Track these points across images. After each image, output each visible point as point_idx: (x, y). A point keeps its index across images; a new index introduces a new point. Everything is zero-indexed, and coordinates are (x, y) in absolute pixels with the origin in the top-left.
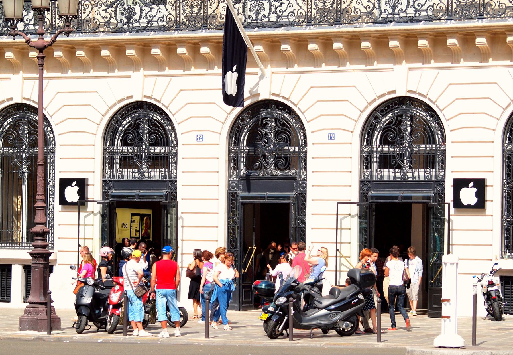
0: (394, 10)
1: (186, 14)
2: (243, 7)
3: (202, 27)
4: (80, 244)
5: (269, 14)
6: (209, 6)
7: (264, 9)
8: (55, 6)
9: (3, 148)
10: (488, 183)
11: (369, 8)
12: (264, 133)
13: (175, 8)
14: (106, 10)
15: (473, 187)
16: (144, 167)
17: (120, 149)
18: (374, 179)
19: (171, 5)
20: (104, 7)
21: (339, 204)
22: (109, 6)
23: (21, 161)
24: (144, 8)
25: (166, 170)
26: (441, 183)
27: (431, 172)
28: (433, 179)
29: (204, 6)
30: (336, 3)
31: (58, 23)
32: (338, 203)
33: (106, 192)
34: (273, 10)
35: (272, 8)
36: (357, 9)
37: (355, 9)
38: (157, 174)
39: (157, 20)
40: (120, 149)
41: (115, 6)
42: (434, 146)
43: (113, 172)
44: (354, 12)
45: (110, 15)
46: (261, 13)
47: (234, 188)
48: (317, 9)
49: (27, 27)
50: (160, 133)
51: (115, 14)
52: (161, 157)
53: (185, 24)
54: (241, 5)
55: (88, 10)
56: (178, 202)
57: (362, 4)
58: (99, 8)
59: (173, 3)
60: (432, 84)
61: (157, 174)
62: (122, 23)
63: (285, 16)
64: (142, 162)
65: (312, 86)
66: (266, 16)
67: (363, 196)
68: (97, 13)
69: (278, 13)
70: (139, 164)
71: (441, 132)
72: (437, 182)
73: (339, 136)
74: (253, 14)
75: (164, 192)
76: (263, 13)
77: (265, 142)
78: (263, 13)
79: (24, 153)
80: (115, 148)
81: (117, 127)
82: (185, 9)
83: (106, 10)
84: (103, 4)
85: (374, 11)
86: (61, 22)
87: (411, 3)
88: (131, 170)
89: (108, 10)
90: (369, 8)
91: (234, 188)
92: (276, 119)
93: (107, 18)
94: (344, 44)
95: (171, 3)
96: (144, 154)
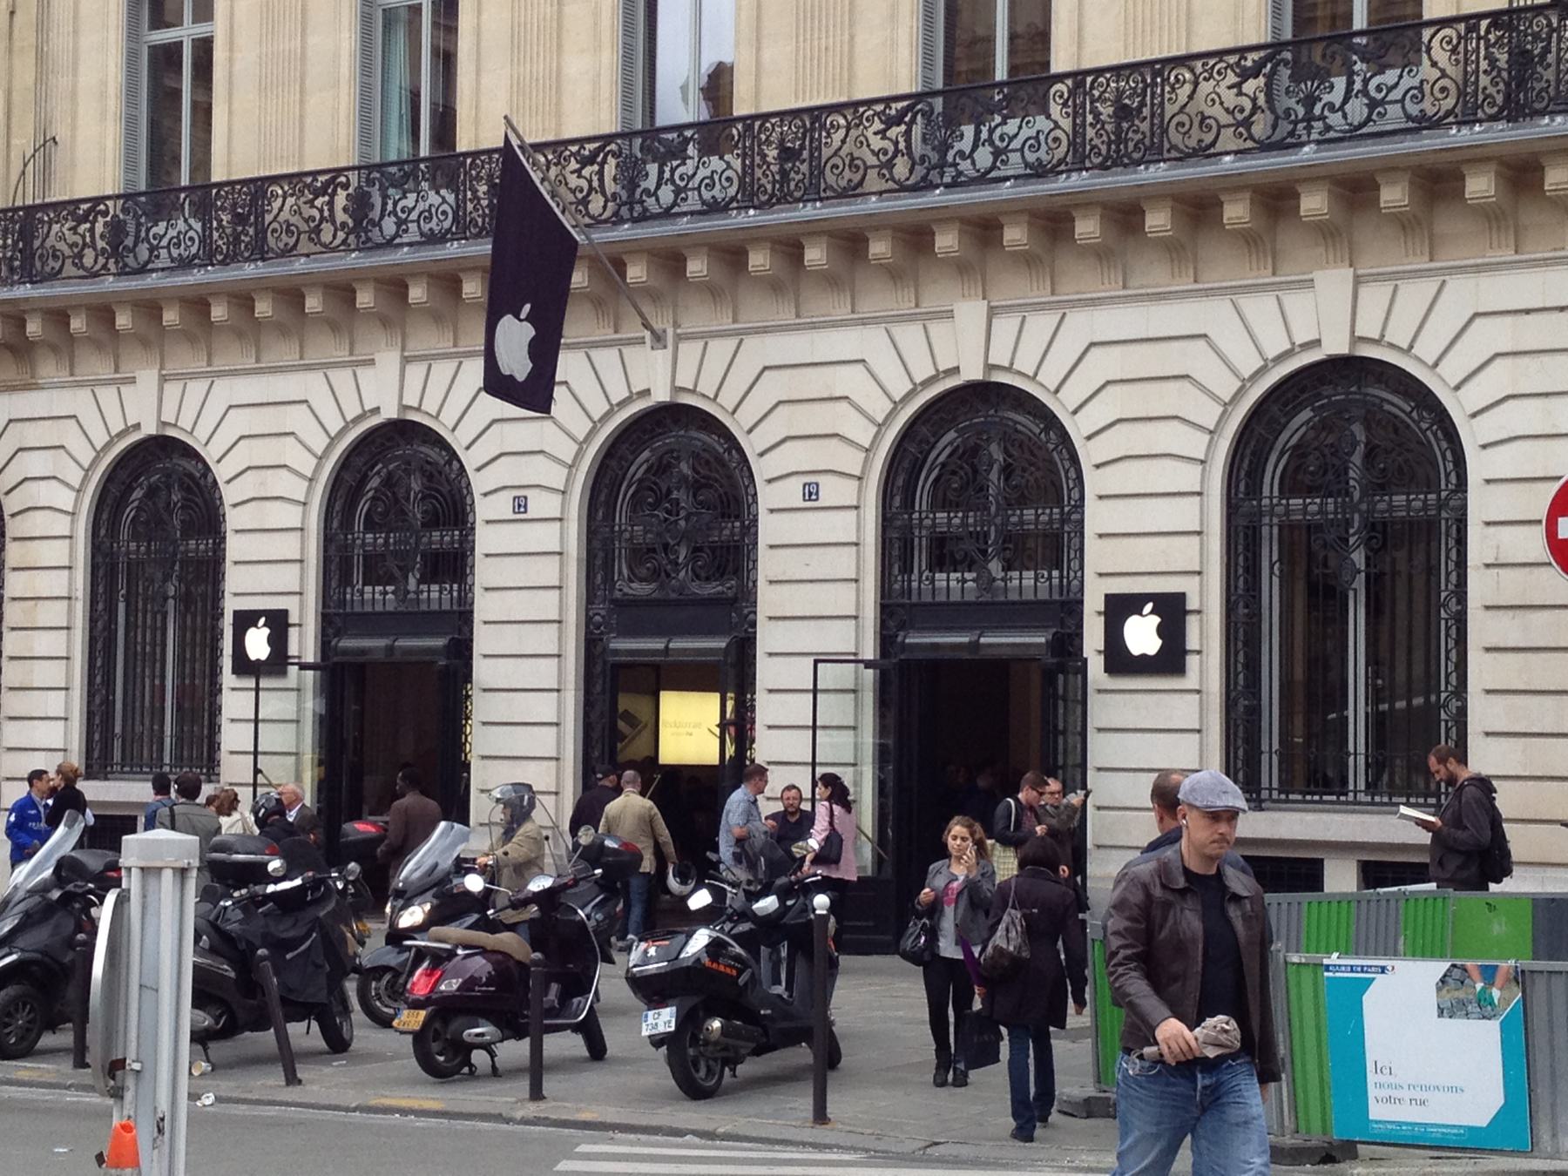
0: (631, 193)
1: (1103, 123)
2: (1269, 85)
3: (1147, 158)
4: (259, 766)
5: (658, 187)
6: (1167, 96)
7: (647, 175)
8: (1478, 34)
9: (632, 526)
10: (1192, 603)
11: (886, 153)
12: (664, 490)
13: (1070, 110)
14: (1238, 85)
15: (1152, 612)
16: (995, 567)
17: (927, 517)
18: (915, 599)
19: (1450, 47)
20: (1232, 78)
21: (819, 665)
22: (1245, 75)
23: (402, 564)
24: (391, 191)
25: (1055, 573)
26: (1072, 608)
27: (1050, 578)
28: (1056, 597)
29: (1153, 97)
30: (1554, 50)
31: (1091, 140)
32: (816, 662)
33: (891, 637)
34: (390, 207)
35: (1354, 82)
36: (1210, 117)
37: (853, 159)
38: (1027, 583)
39: (1399, 97)
40: (927, 517)
41: (599, 159)
42: (737, 524)
43: (910, 581)
44: (1201, 127)
45: (590, 182)
46: (1320, 100)
47: (598, 628)
48: (1494, 73)
49: (1380, 109)
50: (197, 504)
51: (601, 180)
52: (722, 547)
53: (476, 225)
54: (1261, 80)
55: (277, 204)
56: (1086, 659)
57: (1222, 103)
58: (866, 128)
59: (1066, 95)
60: (249, 405)
61: (1027, 583)
62: (926, 164)
63: (412, 221)
64: (1348, 541)
65: (767, 364)
66: (1337, 106)
67: (886, 641)
68: (1213, 100)
69: (1373, 93)
70: (397, 573)
71: (1454, 453)
72: (1063, 603)
73: (831, 490)
74: (1298, 102)
75: (440, 642)
76: (1326, 98)
77: (669, 512)
78: (1326, 98)
79: (1359, 511)
80: (916, 515)
81: (1267, 439)
82: (1101, 109)
83: (578, 172)
84: (1229, 71)
85: (593, 196)
86: (1497, 84)
87: (984, 135)
88: (959, 575)
89: (888, 134)
90: (886, 153)
91: (598, 628)
92: (696, 456)
93: (1242, 110)
94: (1334, 197)
95: (1061, 97)
96: (993, 528)
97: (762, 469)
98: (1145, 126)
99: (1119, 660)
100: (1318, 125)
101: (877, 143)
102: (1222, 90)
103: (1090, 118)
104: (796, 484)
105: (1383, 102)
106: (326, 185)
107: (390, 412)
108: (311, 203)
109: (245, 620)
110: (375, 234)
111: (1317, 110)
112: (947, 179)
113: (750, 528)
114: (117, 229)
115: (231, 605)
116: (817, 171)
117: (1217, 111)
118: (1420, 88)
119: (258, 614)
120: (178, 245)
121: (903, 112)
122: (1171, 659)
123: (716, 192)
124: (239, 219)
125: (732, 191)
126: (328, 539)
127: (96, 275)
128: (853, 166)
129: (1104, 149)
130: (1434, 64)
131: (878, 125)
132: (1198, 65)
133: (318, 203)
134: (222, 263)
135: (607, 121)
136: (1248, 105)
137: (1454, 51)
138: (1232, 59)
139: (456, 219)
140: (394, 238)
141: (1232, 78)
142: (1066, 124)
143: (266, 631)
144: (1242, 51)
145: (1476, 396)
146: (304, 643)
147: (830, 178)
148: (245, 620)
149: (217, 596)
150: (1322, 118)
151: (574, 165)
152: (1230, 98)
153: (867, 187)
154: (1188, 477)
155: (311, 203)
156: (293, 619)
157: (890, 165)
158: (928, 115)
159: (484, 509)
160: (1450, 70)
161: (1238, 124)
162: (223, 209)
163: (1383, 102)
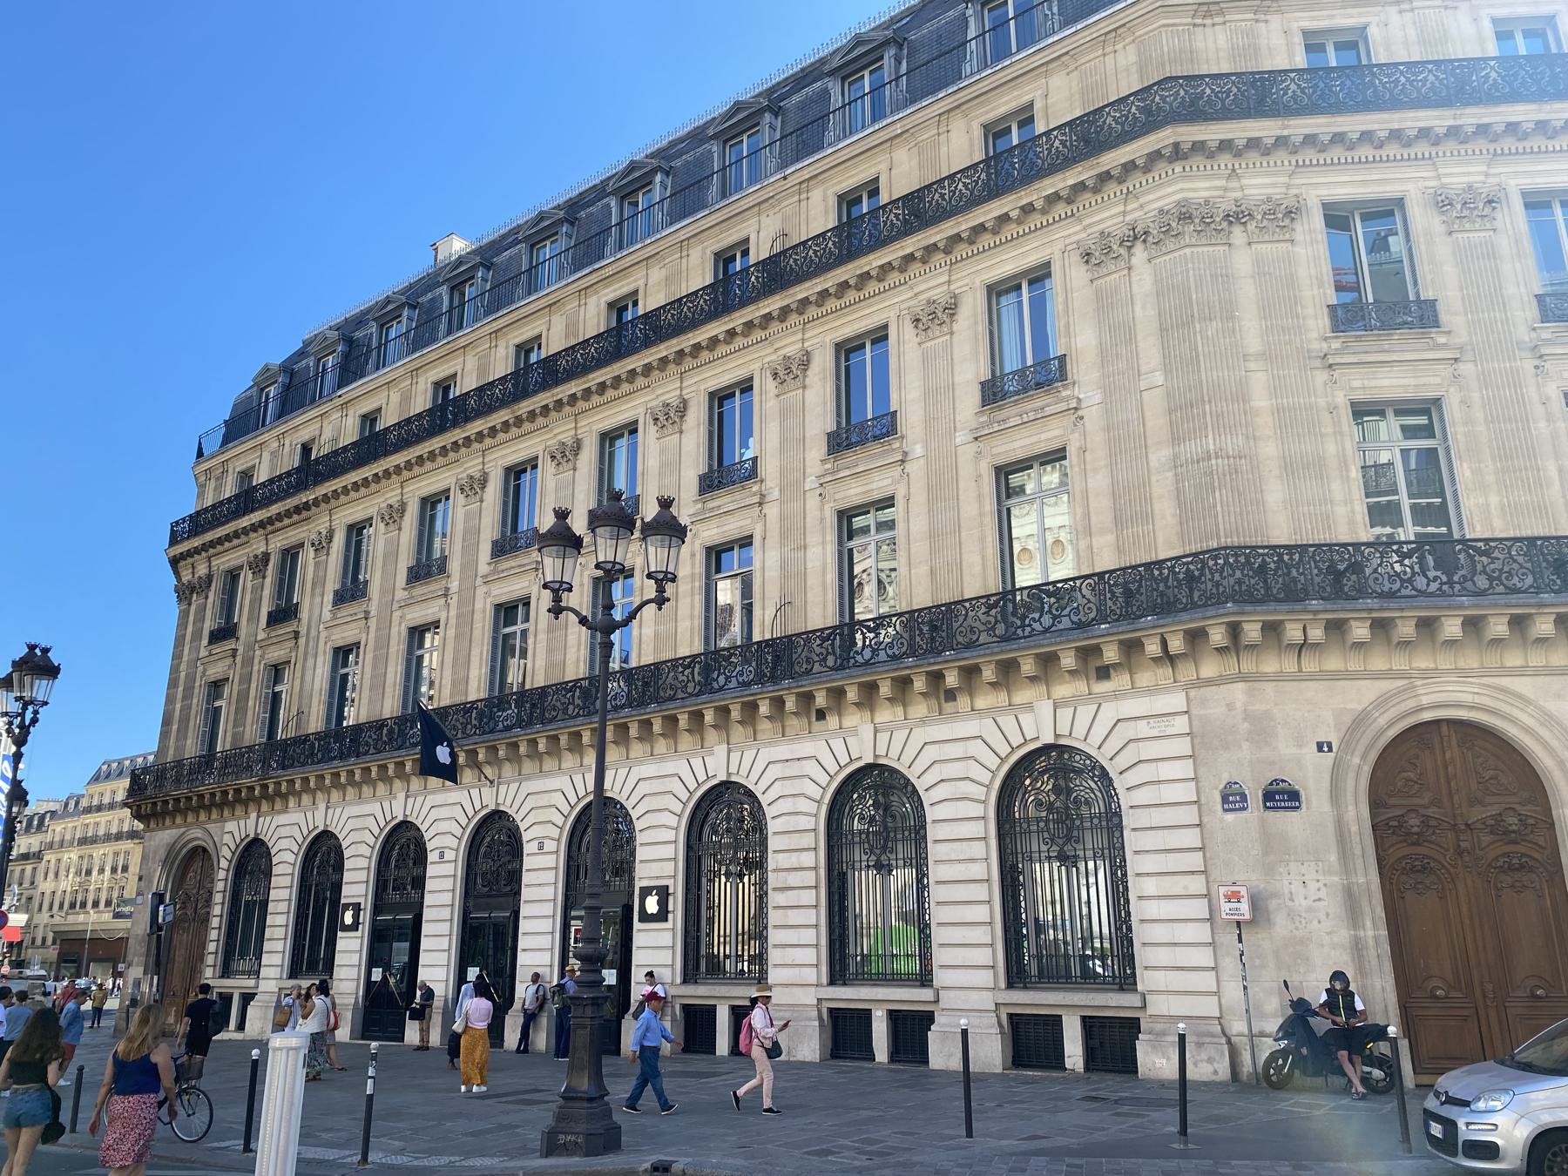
22: (990, 607)
97: (526, 837)
98: (944, 634)
99: (645, 917)
100: (1028, 629)
101: (984, 618)
102: (979, 614)
103: (1108, 595)
104: (536, 842)
105: (1059, 616)
106: (690, 663)
107: (868, 759)
108: (565, 696)
109: (346, 907)
110: (715, 685)
111: (1027, 622)
112: (1026, 634)
113: (633, 853)
114: (391, 731)
115: (638, 884)
116: (951, 636)
117: (978, 624)
118: (1077, 608)
119: (653, 888)
120: (892, 648)
121: (830, 634)
122: (662, 915)
123: (895, 650)
124: (533, 706)
125: (751, 677)
126: (569, 857)
127: (575, 717)
128: (808, 662)
129: (1118, 612)
130: (1084, 597)
131: (818, 642)
132: (967, 605)
133: (825, 645)
134: (638, 706)
135: (697, 647)
136: (993, 620)
137: (1093, 590)
138: (984, 601)
139: (910, 645)
140: (1050, 627)
141: (984, 609)
142: (626, 689)
143: (656, 898)
144: (988, 597)
145: (930, 779)
146: (366, 917)
147: (797, 668)
148: (646, 891)
149: (631, 879)
150: (1030, 625)
151: (681, 669)
152: (984, 618)
153: (981, 640)
154: (978, 810)
155: (565, 696)
156: (671, 891)
157: (825, 659)
158: (841, 635)
159: (432, 857)
160: (1093, 599)
161: (988, 630)
162: (768, 653)
163: (1059, 616)
